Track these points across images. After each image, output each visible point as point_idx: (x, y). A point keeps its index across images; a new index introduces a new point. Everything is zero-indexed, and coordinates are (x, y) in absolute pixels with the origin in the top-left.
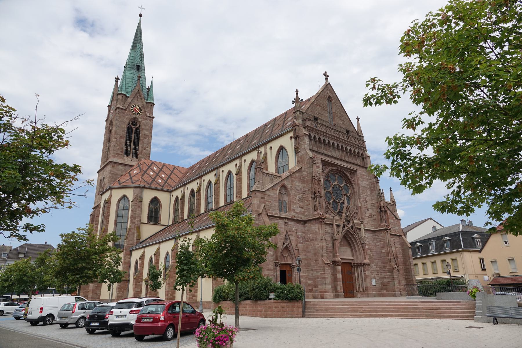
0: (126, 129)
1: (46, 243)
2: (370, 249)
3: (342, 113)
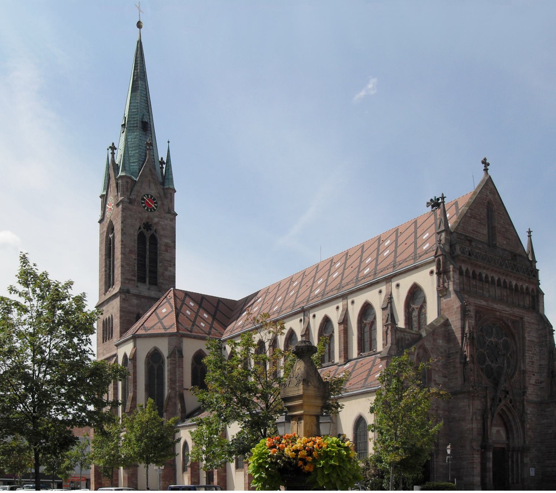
0: (136, 238)
3: (507, 226)
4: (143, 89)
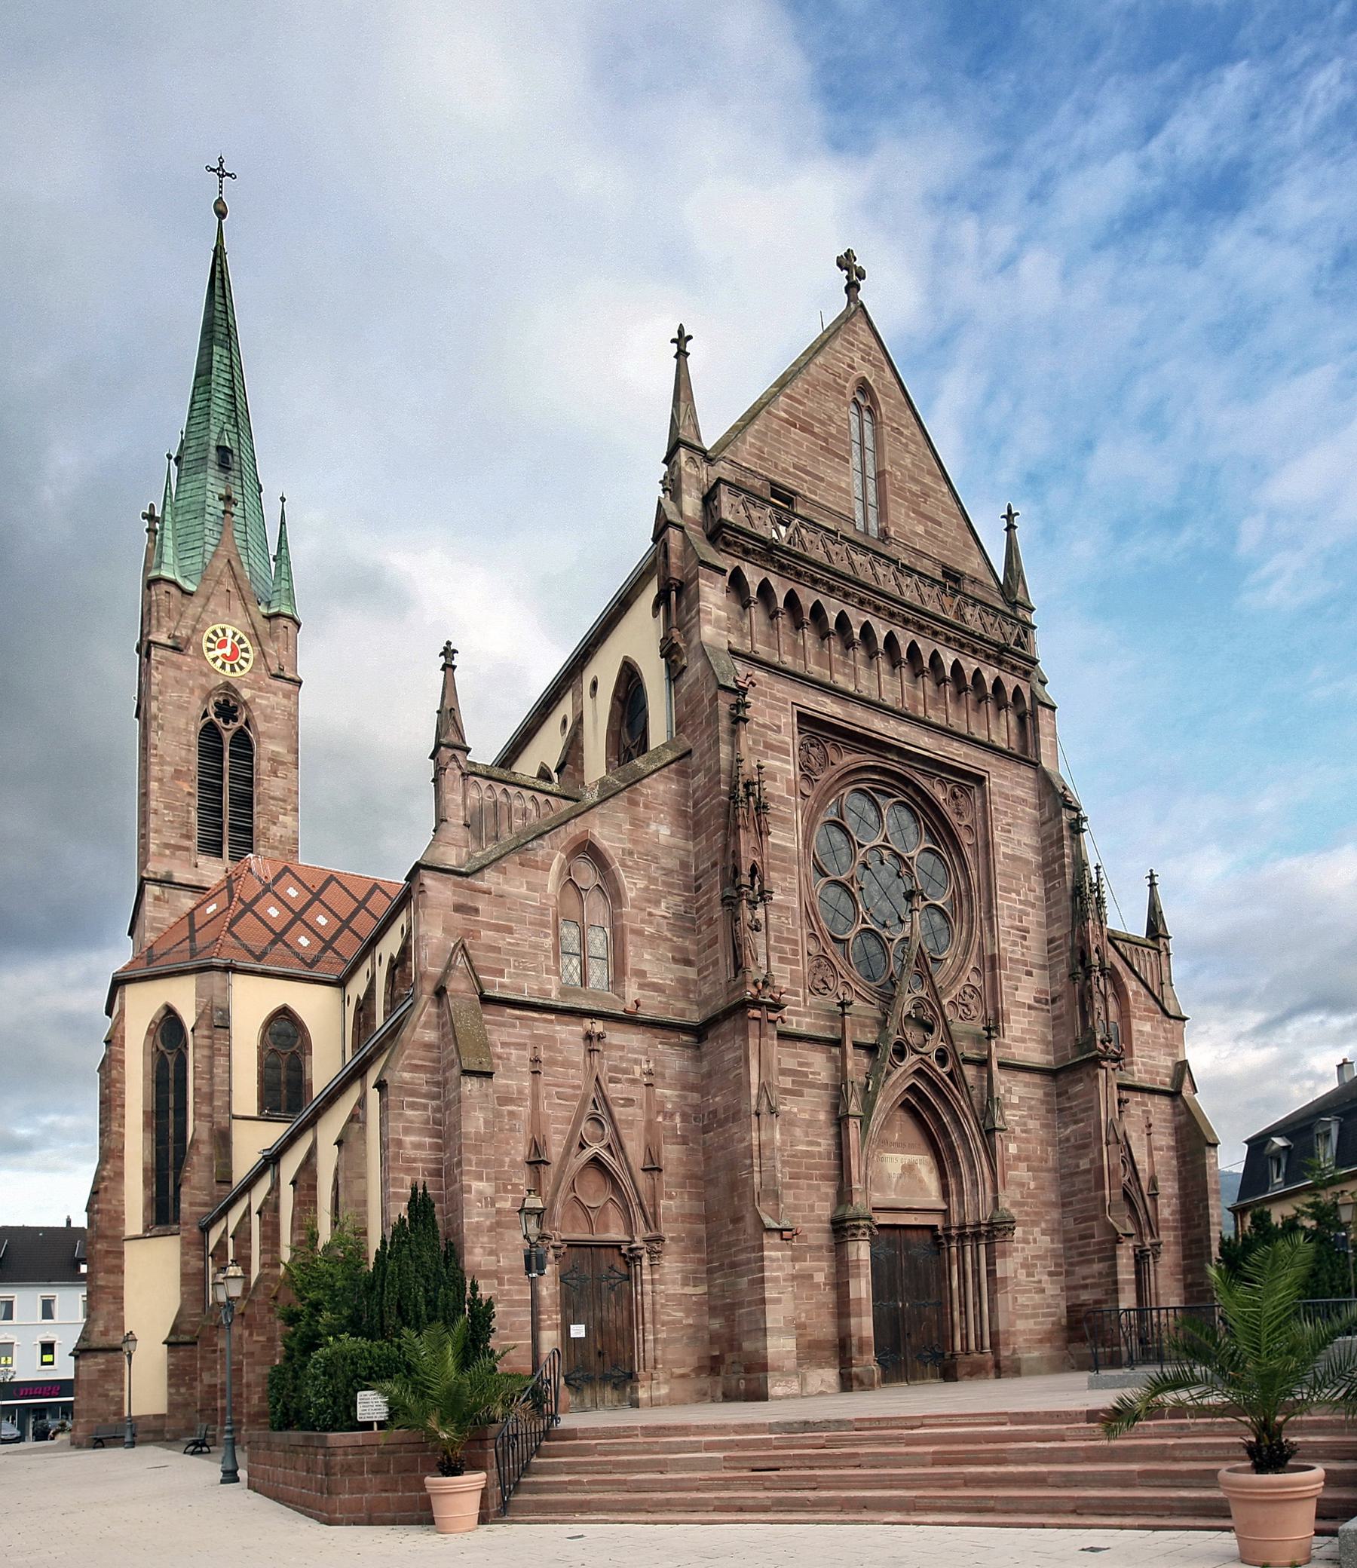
0: (194, 740)
1: (69, 1222)
2: (1027, 1159)
3: (928, 480)
4: (222, 367)
